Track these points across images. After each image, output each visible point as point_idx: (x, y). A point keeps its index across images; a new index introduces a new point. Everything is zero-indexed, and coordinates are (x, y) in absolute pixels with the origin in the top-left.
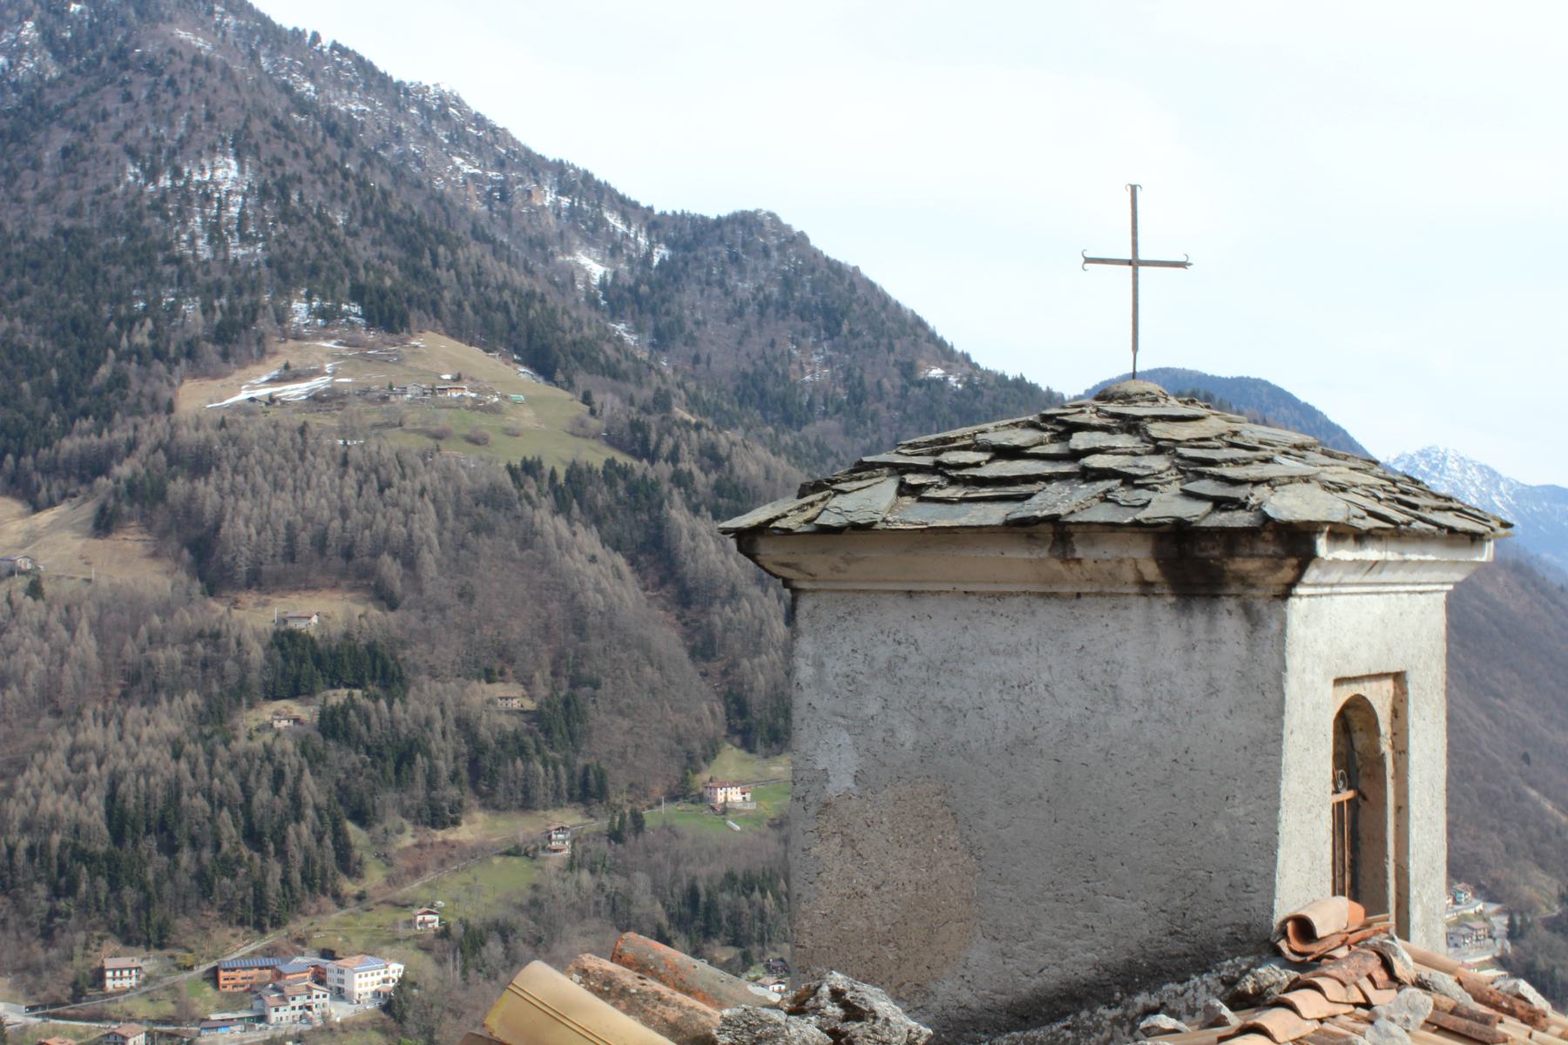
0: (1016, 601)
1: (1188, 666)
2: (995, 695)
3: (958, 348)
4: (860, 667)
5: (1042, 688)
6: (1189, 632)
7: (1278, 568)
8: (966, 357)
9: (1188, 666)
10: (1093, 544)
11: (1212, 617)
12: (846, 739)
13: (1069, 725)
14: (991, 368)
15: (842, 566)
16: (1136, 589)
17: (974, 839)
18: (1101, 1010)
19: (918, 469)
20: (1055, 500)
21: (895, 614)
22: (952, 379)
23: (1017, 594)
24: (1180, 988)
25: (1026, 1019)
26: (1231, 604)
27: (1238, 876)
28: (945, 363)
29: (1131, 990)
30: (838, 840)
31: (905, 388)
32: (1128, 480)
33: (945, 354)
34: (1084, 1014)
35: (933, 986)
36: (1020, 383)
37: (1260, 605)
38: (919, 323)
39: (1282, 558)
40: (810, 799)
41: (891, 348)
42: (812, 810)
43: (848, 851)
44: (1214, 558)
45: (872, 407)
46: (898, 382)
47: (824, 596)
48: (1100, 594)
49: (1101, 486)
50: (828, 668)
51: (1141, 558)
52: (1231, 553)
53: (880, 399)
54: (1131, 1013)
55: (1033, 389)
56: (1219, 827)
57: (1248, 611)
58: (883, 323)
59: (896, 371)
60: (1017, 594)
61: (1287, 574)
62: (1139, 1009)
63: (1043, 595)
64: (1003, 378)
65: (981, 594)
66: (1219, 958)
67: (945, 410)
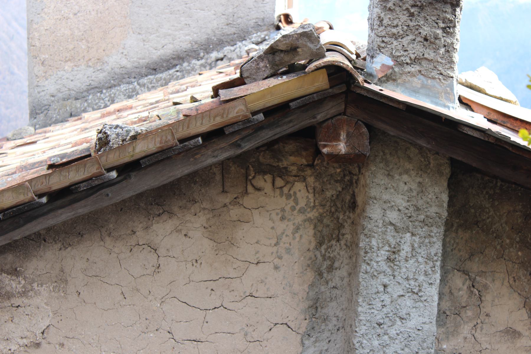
18: (194, 61)
25: (155, 70)
29: (208, 51)
34: (185, 64)
35: (106, 59)
54: (209, 61)
62: (213, 59)
66: (249, 33)
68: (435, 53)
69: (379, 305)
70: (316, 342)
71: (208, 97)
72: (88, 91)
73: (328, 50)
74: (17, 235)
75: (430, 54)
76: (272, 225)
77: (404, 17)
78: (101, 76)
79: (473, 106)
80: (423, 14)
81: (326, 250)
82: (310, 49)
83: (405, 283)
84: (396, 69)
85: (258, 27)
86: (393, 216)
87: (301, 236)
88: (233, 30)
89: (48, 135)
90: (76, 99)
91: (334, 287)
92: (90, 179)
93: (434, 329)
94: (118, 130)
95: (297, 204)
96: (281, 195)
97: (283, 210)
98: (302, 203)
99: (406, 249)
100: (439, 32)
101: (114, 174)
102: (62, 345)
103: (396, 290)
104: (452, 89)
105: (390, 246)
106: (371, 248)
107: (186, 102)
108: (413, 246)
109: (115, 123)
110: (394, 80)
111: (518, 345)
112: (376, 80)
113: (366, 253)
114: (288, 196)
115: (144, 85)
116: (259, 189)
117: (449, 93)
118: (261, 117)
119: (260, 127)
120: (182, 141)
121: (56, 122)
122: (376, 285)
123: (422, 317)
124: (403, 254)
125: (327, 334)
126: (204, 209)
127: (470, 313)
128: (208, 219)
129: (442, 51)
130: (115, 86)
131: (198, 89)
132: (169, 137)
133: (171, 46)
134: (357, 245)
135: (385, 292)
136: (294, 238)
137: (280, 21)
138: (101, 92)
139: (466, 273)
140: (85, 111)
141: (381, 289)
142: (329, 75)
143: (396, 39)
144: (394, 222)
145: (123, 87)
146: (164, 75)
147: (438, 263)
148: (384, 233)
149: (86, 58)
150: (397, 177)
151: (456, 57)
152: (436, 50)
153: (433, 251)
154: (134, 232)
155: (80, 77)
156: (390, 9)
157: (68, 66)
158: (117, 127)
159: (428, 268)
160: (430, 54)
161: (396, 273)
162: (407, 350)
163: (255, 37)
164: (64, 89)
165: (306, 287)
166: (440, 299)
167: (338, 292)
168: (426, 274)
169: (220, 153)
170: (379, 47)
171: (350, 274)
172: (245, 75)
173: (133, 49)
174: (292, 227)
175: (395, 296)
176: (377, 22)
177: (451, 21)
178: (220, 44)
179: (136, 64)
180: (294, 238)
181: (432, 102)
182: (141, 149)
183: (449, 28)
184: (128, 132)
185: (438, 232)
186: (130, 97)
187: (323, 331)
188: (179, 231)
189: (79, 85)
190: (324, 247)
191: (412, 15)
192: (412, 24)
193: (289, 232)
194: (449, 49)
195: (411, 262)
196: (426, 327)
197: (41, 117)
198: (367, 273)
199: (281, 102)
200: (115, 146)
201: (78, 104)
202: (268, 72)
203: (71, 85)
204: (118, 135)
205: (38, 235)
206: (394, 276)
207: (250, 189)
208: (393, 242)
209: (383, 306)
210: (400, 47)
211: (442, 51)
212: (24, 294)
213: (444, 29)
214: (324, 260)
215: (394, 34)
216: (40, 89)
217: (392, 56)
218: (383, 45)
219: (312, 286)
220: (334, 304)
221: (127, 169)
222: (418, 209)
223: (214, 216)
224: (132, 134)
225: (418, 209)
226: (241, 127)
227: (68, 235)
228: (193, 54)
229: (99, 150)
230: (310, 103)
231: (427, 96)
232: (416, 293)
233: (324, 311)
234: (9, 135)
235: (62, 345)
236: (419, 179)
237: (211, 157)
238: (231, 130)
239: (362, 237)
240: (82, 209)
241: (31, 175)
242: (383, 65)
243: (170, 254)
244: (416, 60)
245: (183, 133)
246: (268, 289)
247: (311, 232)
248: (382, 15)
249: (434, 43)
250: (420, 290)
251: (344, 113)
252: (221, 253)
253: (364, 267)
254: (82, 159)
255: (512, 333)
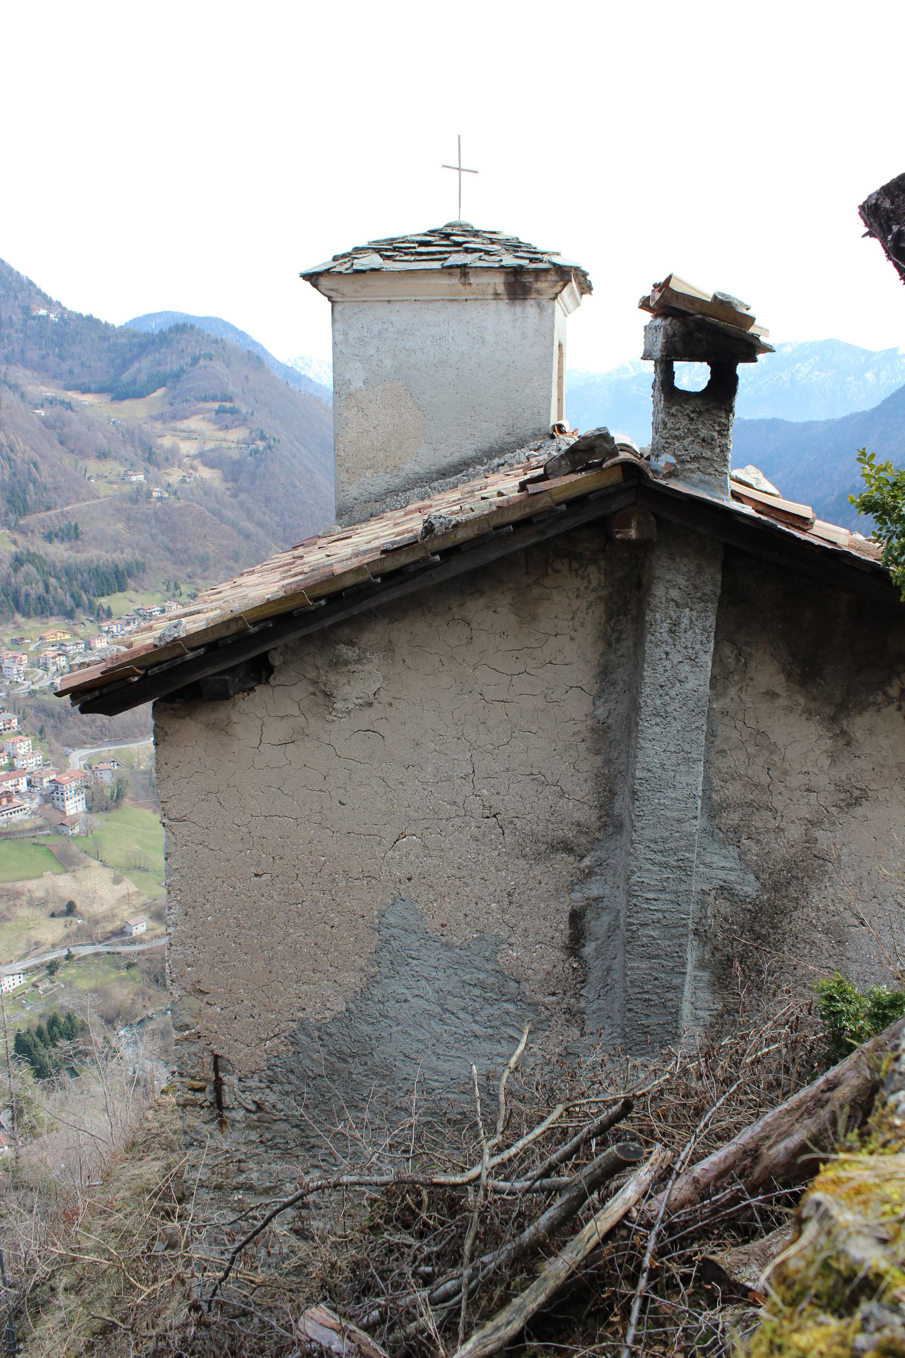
0: (438, 303)
1: (514, 328)
2: (429, 343)
3: (54, 299)
4: (365, 334)
5: (450, 339)
6: (515, 314)
7: (555, 286)
8: (59, 304)
9: (514, 328)
10: (478, 277)
11: (524, 308)
12: (359, 365)
13: (463, 354)
14: (74, 310)
15: (359, 289)
16: (492, 297)
17: (420, 403)
18: (478, 467)
19: (386, 250)
20: (456, 259)
21: (382, 310)
22: (52, 316)
23: (439, 300)
24: (512, 455)
25: (444, 475)
26: (532, 302)
27: (535, 410)
28: (47, 306)
29: (490, 458)
30: (356, 409)
31: (25, 321)
32: (487, 253)
33: (48, 302)
34: (471, 470)
35: (402, 466)
36: (90, 318)
37: (544, 302)
38: (31, 283)
39: (557, 282)
40: (342, 392)
41: (16, 298)
42: (343, 397)
43: (361, 414)
44: (530, 282)
45: (7, 331)
46: (21, 317)
47: (347, 304)
48: (476, 300)
49: (477, 255)
50: (350, 334)
51: (498, 282)
52: (537, 279)
53: (12, 327)
54: (492, 467)
55: (97, 322)
56: (528, 391)
57: (539, 305)
58: (10, 283)
59: (19, 311)
60: (439, 300)
61: (558, 289)
62: (496, 464)
63: (450, 300)
64: (81, 315)
65: (422, 301)
66: (527, 442)
67: (49, 333)
68: (713, 452)
69: (662, 670)
70: (605, 702)
71: (513, 492)
72: (385, 494)
73: (621, 450)
74: (355, 611)
75: (707, 454)
76: (568, 602)
77: (685, 422)
78: (398, 481)
79: (743, 499)
80: (701, 419)
81: (615, 624)
82: (605, 448)
83: (684, 651)
84: (678, 467)
85: (535, 436)
86: (674, 594)
87: (593, 612)
88: (513, 439)
89: (358, 531)
90: (376, 501)
91: (622, 656)
92: (417, 562)
93: (708, 690)
94: (442, 520)
95: (590, 584)
96: (577, 576)
97: (578, 589)
98: (595, 583)
99: (685, 621)
100: (715, 434)
101: (438, 557)
102: (391, 704)
103: (676, 658)
104: (726, 483)
105: (671, 619)
106: (655, 621)
107: (492, 497)
108: (691, 619)
109: (437, 514)
110: (676, 476)
111: (777, 704)
112: (661, 476)
113: (651, 625)
114: (583, 578)
115: (435, 489)
116: (558, 571)
117: (723, 487)
118: (563, 507)
119: (562, 517)
120: (496, 528)
121: (360, 522)
122: (659, 653)
123: (698, 680)
124: (683, 626)
125: (614, 696)
126: (511, 588)
127: (736, 678)
128: (514, 598)
129: (718, 450)
130: (409, 489)
131: (503, 486)
132: (486, 525)
133: (459, 454)
134: (643, 618)
135: (667, 659)
136: (587, 614)
137: (554, 431)
138: (398, 495)
139: (734, 643)
140: (383, 512)
141: (664, 656)
142: (623, 471)
143: (678, 440)
144: (675, 598)
145: (416, 491)
146: (452, 479)
147: (712, 634)
148: (667, 608)
149: (385, 466)
150: (678, 560)
151: (730, 456)
152: (712, 449)
153: (708, 624)
154: (450, 609)
155: (379, 482)
156: (673, 415)
157: (368, 473)
158: (440, 517)
159: (704, 638)
160: (707, 454)
161: (677, 643)
162: (684, 708)
163: (532, 445)
164: (365, 493)
165: (597, 655)
166: (713, 666)
167: (625, 660)
168: (702, 643)
169: (529, 539)
170: (663, 447)
171: (635, 644)
172: (549, 471)
173: (424, 457)
174: (585, 604)
175: (675, 662)
176: (661, 426)
177: (725, 425)
178: (502, 451)
179: (428, 470)
180: (587, 614)
181: (709, 495)
182: (462, 535)
183: (724, 430)
184: (450, 521)
185: (712, 607)
186: (422, 499)
187: (612, 693)
188: (488, 608)
189: (378, 489)
190: (613, 620)
191: (691, 419)
192: (692, 427)
193: (584, 609)
194: (724, 449)
195: (690, 633)
196: (701, 689)
197: (346, 517)
198: (651, 642)
199: (577, 494)
200: (440, 533)
201: (377, 505)
202: (569, 469)
203: (372, 489)
204: (441, 523)
205: (370, 611)
206: (675, 645)
207: (550, 571)
208: (674, 616)
209: (666, 671)
210: (681, 447)
211: (718, 450)
212: (358, 661)
213: (719, 432)
214: (613, 632)
215: (676, 436)
216: (344, 494)
217: (675, 455)
218: (667, 445)
219: (603, 654)
220: (621, 670)
221: (448, 553)
222: (696, 588)
223: (519, 595)
224: (453, 523)
225: (696, 588)
226: (547, 516)
227: (396, 611)
228: (478, 461)
229: (425, 537)
230: (604, 495)
231: (704, 489)
232: (693, 660)
233: (613, 676)
234: (320, 534)
235: (391, 704)
236: (696, 562)
237: (519, 544)
238: (539, 519)
239: (648, 611)
240: (410, 588)
241: (367, 559)
242: (667, 463)
243: (481, 627)
244: (696, 459)
245: (496, 521)
246: (565, 658)
247: (603, 608)
248: (666, 420)
249: (711, 444)
250: (697, 657)
251: (635, 505)
252: (525, 626)
253: (649, 637)
254: (410, 546)
255: (772, 695)
